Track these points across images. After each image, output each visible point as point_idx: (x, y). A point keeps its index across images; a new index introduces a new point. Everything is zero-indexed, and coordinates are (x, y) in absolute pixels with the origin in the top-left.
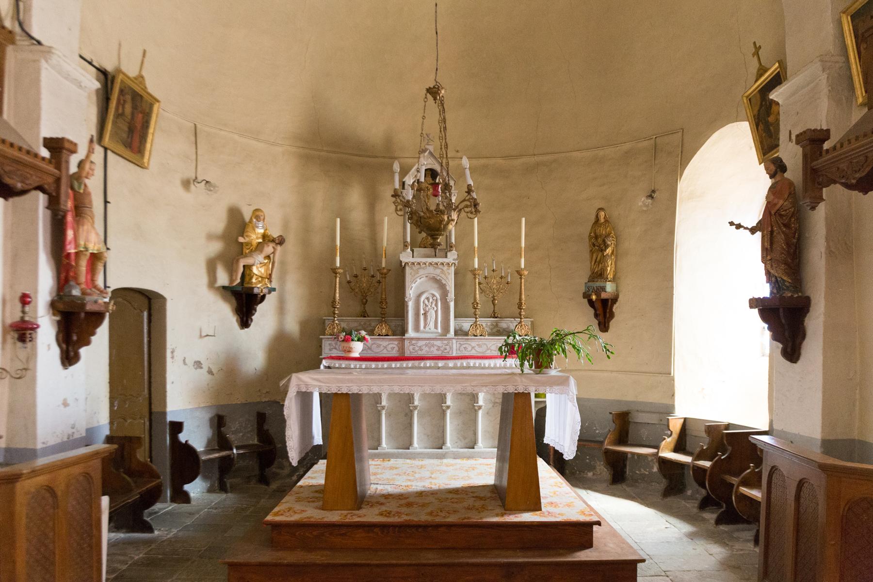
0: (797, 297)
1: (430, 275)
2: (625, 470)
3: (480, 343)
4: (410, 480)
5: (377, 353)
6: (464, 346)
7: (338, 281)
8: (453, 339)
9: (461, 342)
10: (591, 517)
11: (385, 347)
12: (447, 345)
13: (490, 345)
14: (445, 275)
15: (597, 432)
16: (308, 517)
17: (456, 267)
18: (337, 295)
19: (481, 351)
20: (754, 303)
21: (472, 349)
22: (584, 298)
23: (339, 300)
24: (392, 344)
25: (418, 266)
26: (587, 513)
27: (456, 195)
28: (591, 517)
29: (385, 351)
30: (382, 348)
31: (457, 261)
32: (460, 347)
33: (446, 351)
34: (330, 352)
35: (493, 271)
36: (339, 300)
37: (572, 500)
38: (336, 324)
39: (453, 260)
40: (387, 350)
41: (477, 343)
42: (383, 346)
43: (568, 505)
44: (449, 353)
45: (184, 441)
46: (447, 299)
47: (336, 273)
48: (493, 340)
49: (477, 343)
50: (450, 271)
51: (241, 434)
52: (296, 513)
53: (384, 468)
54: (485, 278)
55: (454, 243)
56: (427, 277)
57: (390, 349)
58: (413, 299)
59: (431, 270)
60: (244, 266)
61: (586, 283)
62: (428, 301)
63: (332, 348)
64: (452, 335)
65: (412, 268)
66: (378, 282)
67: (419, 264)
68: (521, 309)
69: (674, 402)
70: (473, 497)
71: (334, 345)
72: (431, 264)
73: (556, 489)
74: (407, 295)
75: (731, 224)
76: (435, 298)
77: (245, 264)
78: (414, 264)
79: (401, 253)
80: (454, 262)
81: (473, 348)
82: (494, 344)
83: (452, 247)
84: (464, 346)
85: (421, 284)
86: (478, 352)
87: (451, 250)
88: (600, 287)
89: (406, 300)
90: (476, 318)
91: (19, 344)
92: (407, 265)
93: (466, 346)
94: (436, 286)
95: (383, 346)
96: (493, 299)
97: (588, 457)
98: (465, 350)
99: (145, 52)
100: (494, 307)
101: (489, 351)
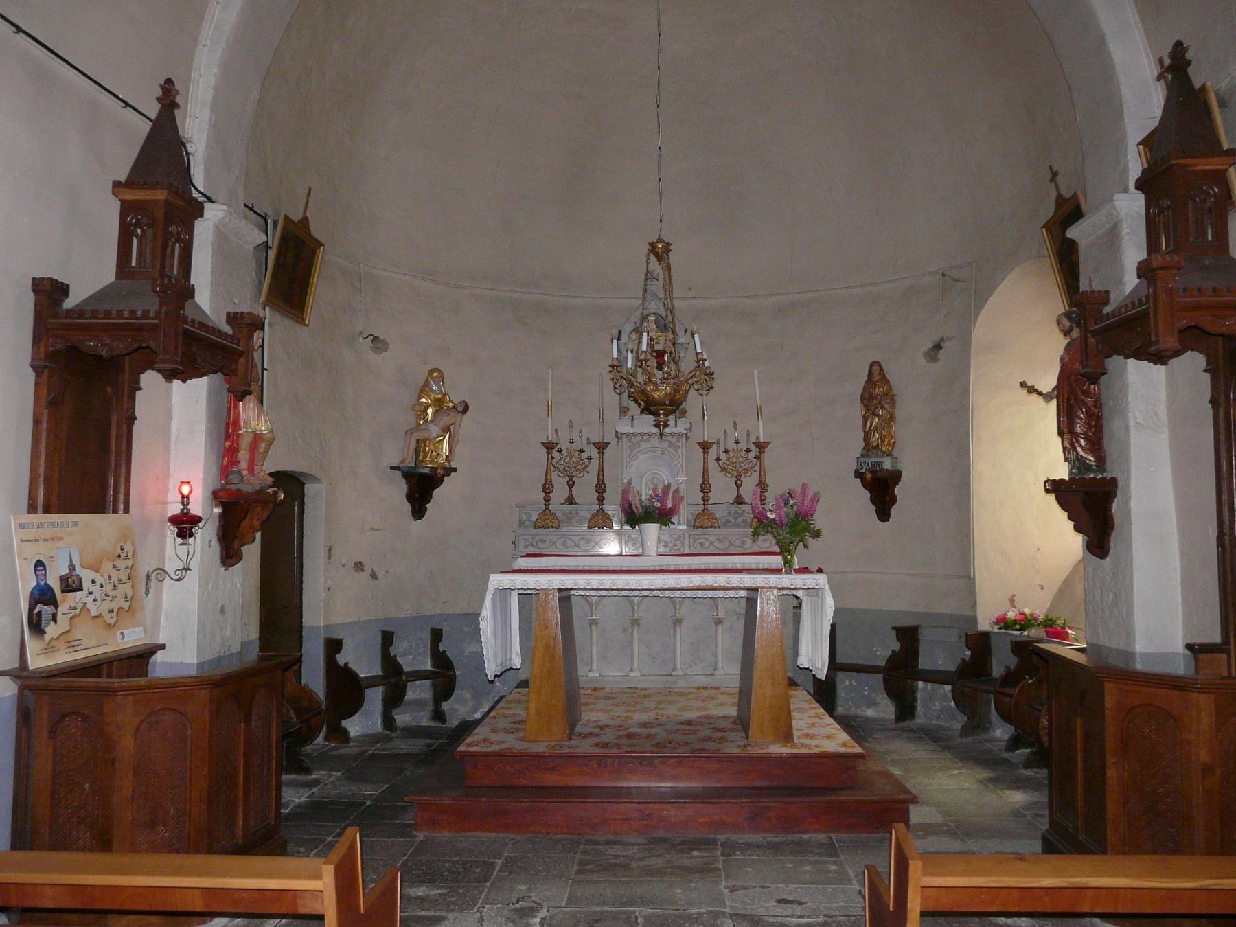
0: (1101, 478)
2: (915, 704)
4: (630, 711)
10: (854, 750)
12: (677, 540)
13: (734, 540)
15: (878, 653)
16: (507, 749)
20: (1054, 487)
22: (856, 477)
26: (849, 744)
28: (854, 750)
37: (834, 731)
43: (828, 737)
45: (342, 664)
51: (411, 657)
52: (492, 744)
53: (597, 698)
60: (418, 441)
61: (858, 458)
63: (528, 545)
69: (976, 613)
70: (711, 728)
71: (530, 540)
73: (817, 720)
75: (1023, 385)
77: (418, 438)
80: (685, 432)
81: (712, 543)
82: (740, 538)
86: (716, 548)
88: (877, 462)
91: (179, 540)
93: (703, 540)
97: (866, 688)
99: (310, 190)
101: (732, 547)
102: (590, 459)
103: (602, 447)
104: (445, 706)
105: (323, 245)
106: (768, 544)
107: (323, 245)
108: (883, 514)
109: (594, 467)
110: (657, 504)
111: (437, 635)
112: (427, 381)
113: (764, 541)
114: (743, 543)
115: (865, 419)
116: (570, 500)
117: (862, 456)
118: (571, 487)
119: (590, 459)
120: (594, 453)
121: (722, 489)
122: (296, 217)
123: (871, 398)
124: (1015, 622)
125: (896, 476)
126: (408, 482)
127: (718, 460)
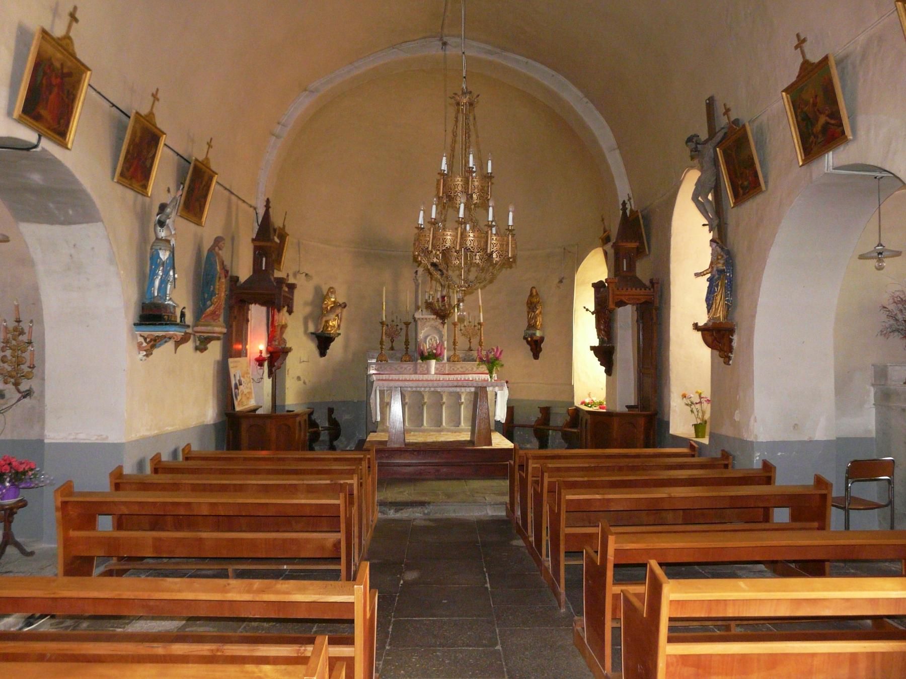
20: (592, 348)
75: (585, 308)
81: (458, 369)
91: (259, 367)
102: (401, 329)
103: (407, 324)
104: (335, 443)
105: (88, 69)
106: (483, 369)
107: (165, 134)
108: (536, 356)
109: (403, 333)
110: (434, 351)
111: (331, 411)
112: (328, 293)
113: (482, 368)
114: (473, 369)
115: (528, 313)
116: (392, 349)
117: (527, 329)
118: (392, 342)
119: (401, 329)
120: (404, 327)
121: (462, 342)
122: (144, 111)
123: (531, 303)
124: (589, 403)
125: (542, 339)
126: (318, 340)
127: (461, 330)
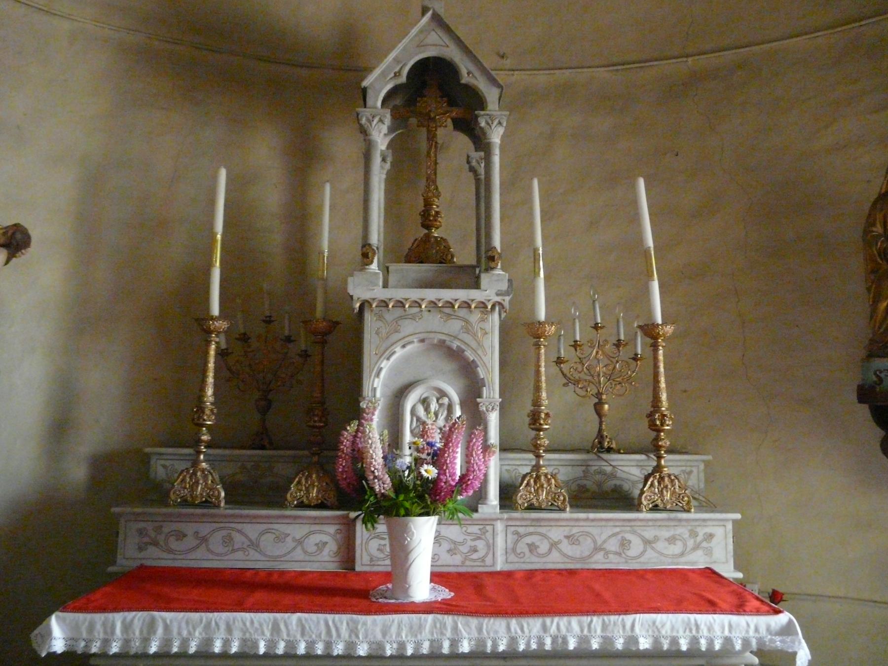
1: (432, 335)
3: (575, 530)
5: (275, 559)
6: (529, 540)
7: (661, 358)
8: (497, 519)
9: (522, 530)
11: (300, 542)
12: (479, 538)
13: (604, 537)
14: (474, 335)
17: (503, 315)
18: (210, 391)
19: (578, 554)
21: (550, 550)
23: (212, 404)
24: (320, 532)
25: (399, 312)
27: (505, 124)
29: (298, 554)
30: (290, 543)
31: (507, 298)
32: (516, 542)
33: (475, 556)
34: (141, 555)
35: (596, 327)
36: (212, 404)
38: (203, 471)
39: (497, 295)
40: (305, 552)
41: (566, 531)
42: (294, 540)
44: (483, 561)
46: (478, 404)
47: (209, 332)
48: (611, 523)
49: (566, 531)
50: (487, 326)
54: (576, 345)
55: (499, 250)
56: (422, 341)
57: (312, 549)
58: (381, 403)
59: (433, 322)
62: (427, 409)
63: (146, 544)
64: (494, 507)
65: (380, 318)
66: (300, 356)
67: (400, 304)
68: (539, 430)
72: (433, 304)
74: (367, 391)
76: (446, 401)
78: (387, 306)
79: (352, 275)
80: (498, 299)
81: (554, 545)
83: (492, 259)
84: (529, 540)
85: (406, 360)
87: (492, 269)
89: (363, 405)
90: (659, 457)
92: (366, 304)
94: (449, 366)
95: (294, 540)
96: (597, 400)
98: (531, 551)
100: (601, 423)
101: (599, 556)
